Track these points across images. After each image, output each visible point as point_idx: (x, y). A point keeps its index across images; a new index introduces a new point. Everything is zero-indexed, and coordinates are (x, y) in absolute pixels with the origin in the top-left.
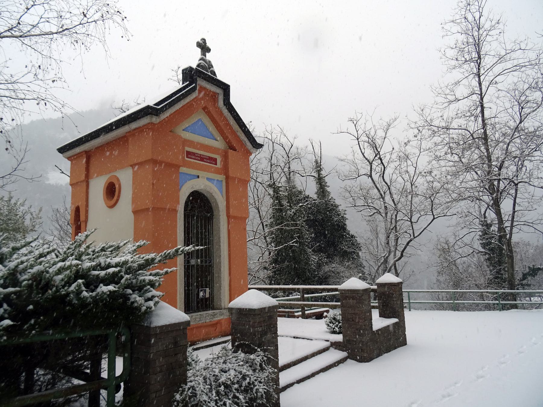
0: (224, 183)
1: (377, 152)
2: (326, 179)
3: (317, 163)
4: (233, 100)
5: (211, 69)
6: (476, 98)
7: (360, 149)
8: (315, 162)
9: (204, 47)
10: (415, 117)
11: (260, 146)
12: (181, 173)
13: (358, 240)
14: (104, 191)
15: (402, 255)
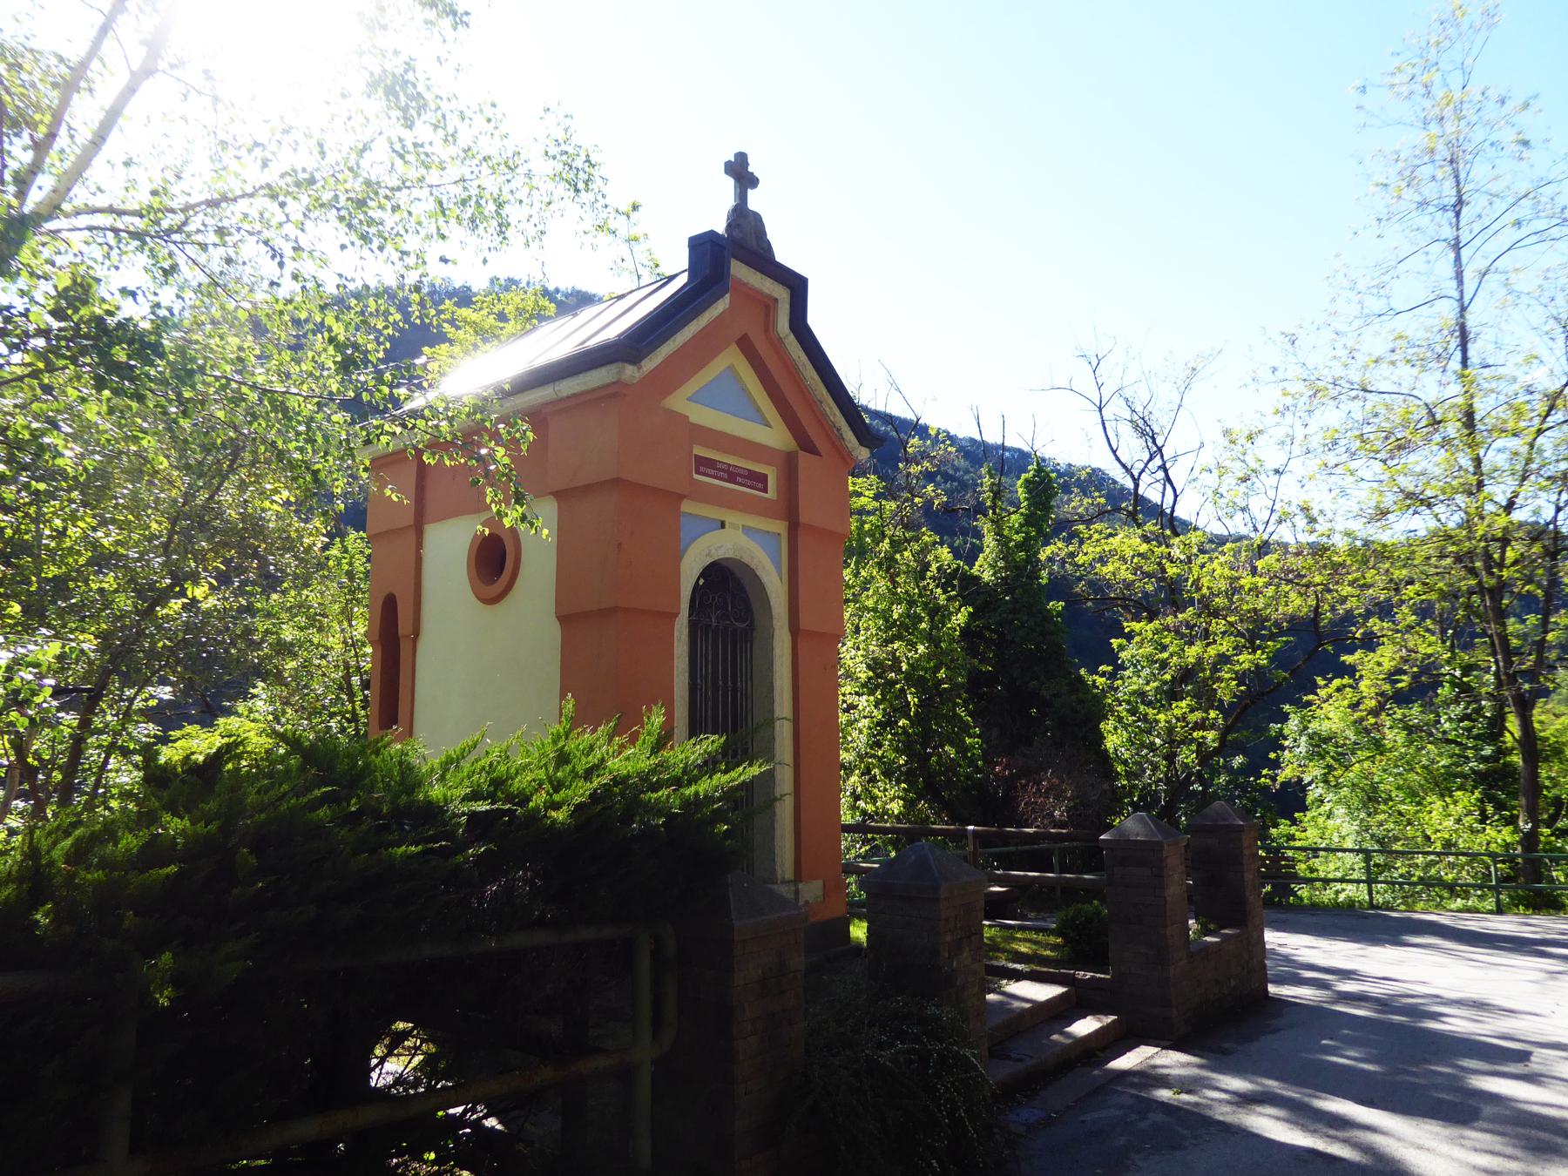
1: (1155, 449)
4: (816, 320)
6: (1448, 310)
9: (741, 173)
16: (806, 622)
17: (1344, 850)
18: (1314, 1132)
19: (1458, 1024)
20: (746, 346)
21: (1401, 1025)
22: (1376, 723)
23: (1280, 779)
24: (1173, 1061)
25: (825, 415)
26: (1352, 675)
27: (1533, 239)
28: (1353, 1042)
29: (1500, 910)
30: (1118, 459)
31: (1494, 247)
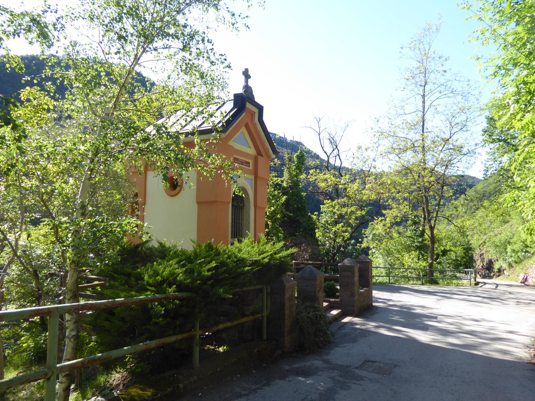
4: (265, 119)
6: (420, 114)
16: (259, 204)
17: (380, 268)
18: (394, 333)
19: (419, 311)
20: (247, 126)
21: (406, 311)
22: (390, 231)
23: (362, 247)
24: (356, 320)
25: (265, 145)
26: (384, 217)
27: (444, 96)
28: (396, 315)
29: (423, 284)
30: (341, 161)
31: (433, 98)
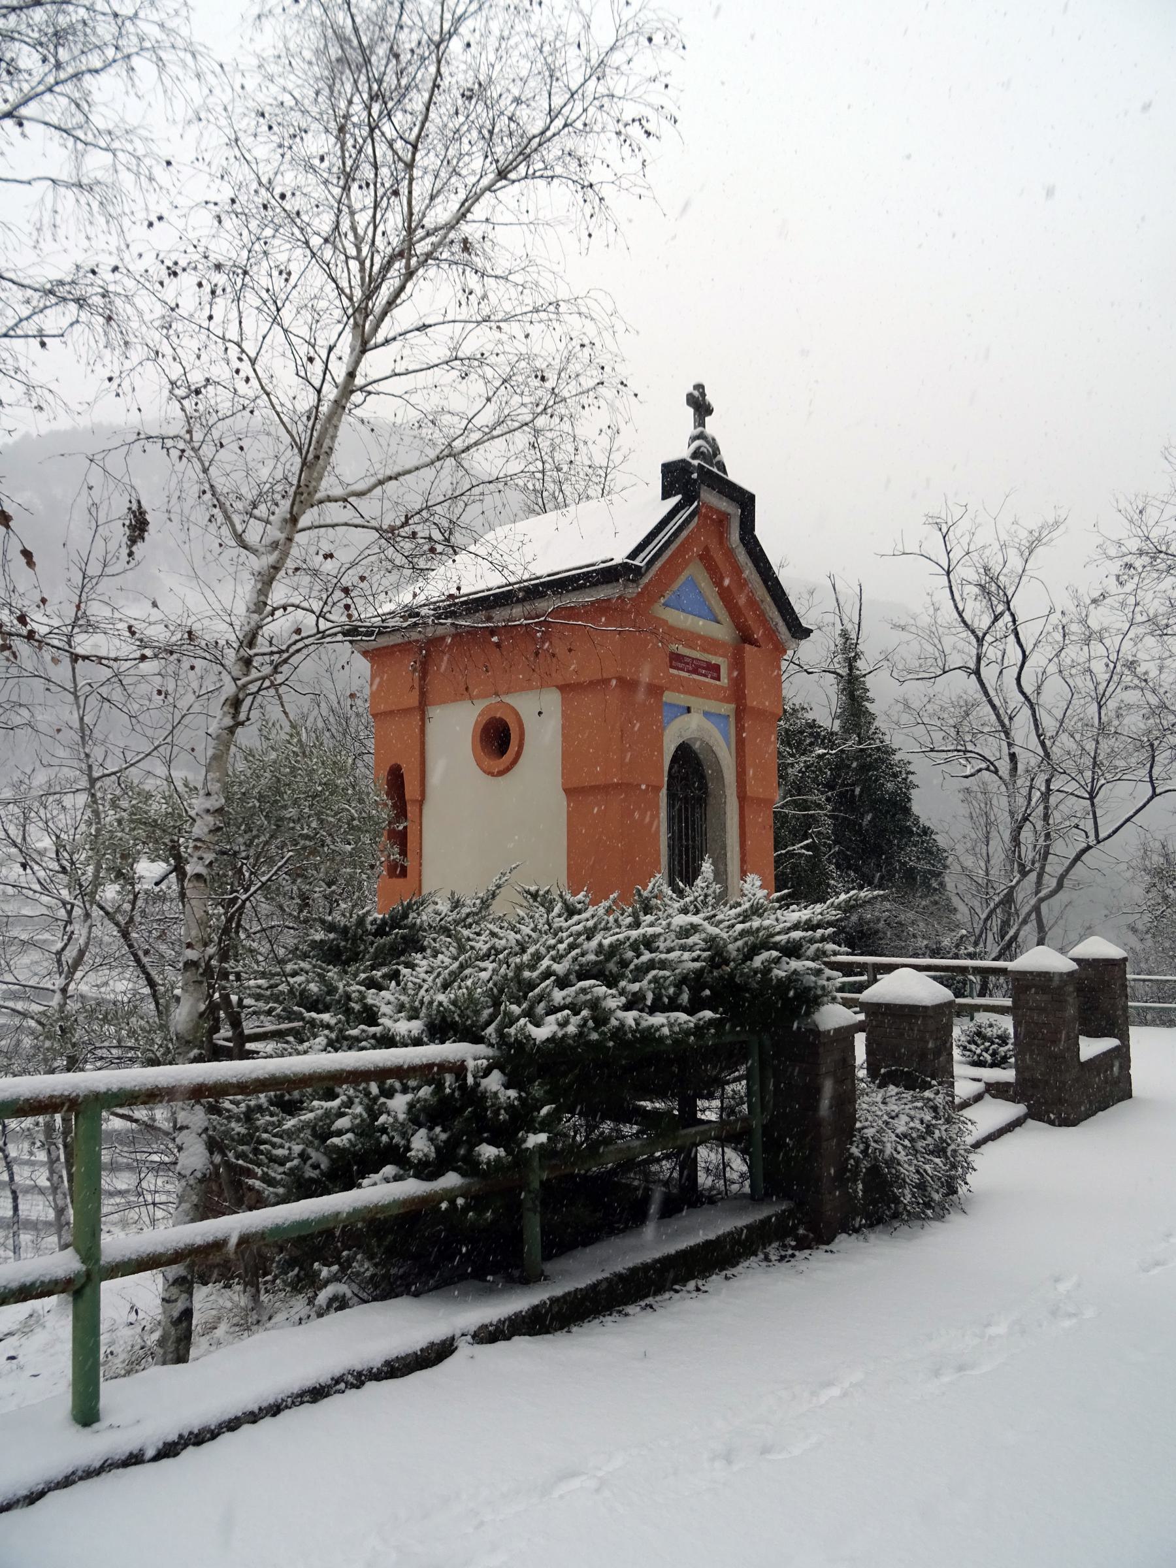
0: (732, 720)
2: (869, 682)
3: (847, 639)
4: (761, 531)
5: (718, 458)
7: (954, 600)
8: (840, 635)
9: (700, 406)
10: (1118, 528)
11: (807, 633)
12: (666, 703)
13: (941, 840)
14: (473, 737)
15: (1060, 886)
20: (706, 558)
